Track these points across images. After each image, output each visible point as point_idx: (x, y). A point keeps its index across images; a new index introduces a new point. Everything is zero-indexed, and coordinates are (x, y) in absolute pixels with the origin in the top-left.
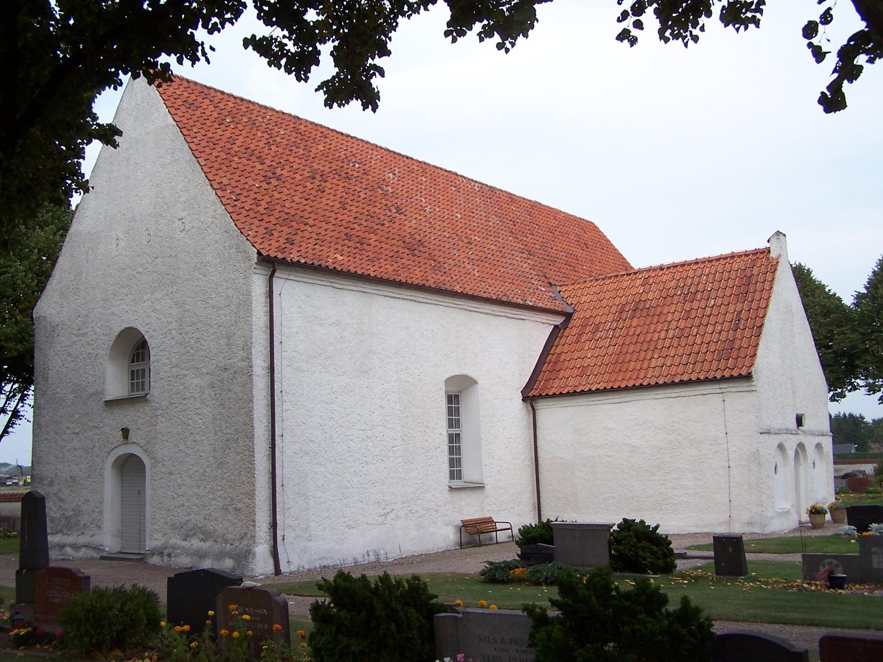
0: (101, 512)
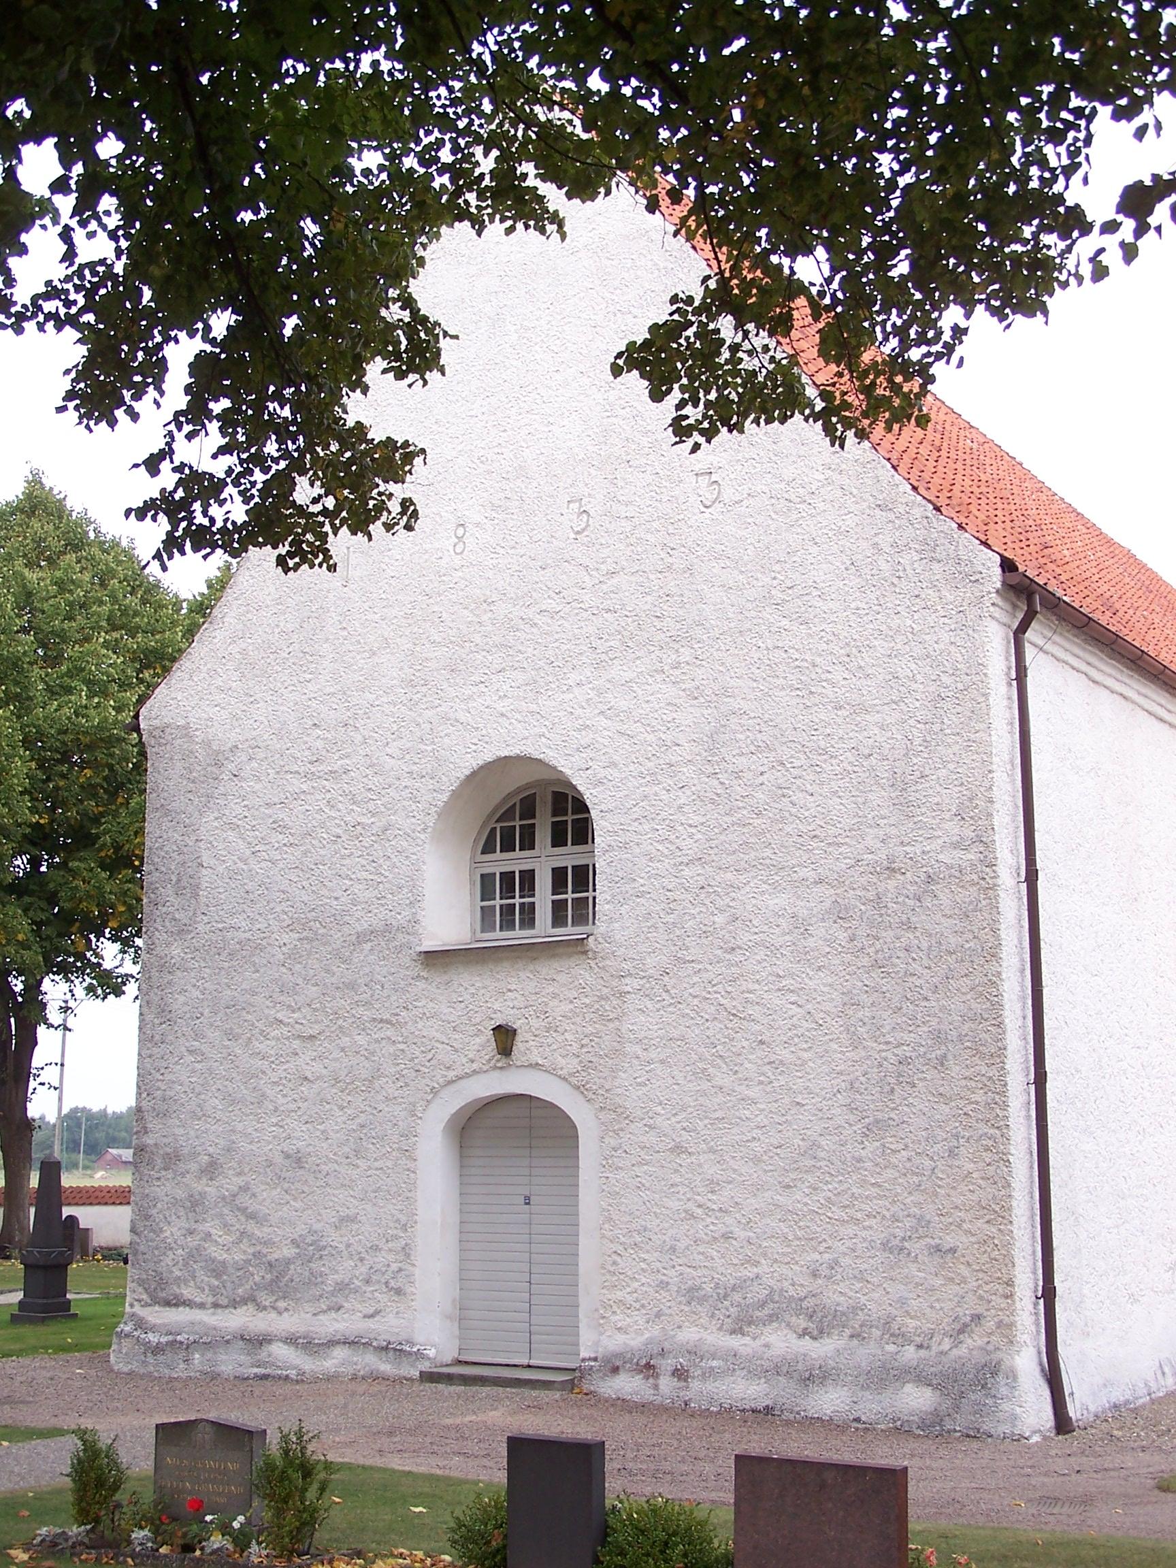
0: (406, 1251)
